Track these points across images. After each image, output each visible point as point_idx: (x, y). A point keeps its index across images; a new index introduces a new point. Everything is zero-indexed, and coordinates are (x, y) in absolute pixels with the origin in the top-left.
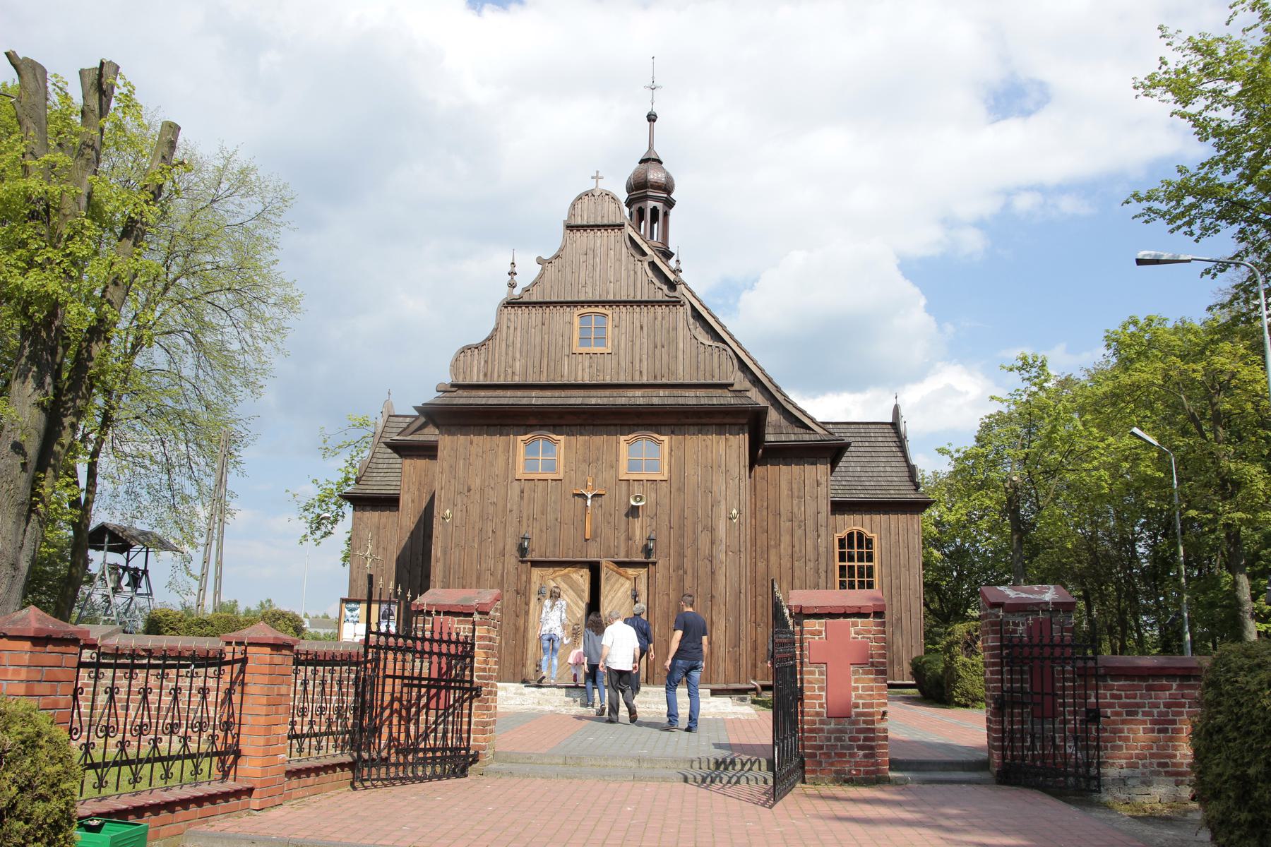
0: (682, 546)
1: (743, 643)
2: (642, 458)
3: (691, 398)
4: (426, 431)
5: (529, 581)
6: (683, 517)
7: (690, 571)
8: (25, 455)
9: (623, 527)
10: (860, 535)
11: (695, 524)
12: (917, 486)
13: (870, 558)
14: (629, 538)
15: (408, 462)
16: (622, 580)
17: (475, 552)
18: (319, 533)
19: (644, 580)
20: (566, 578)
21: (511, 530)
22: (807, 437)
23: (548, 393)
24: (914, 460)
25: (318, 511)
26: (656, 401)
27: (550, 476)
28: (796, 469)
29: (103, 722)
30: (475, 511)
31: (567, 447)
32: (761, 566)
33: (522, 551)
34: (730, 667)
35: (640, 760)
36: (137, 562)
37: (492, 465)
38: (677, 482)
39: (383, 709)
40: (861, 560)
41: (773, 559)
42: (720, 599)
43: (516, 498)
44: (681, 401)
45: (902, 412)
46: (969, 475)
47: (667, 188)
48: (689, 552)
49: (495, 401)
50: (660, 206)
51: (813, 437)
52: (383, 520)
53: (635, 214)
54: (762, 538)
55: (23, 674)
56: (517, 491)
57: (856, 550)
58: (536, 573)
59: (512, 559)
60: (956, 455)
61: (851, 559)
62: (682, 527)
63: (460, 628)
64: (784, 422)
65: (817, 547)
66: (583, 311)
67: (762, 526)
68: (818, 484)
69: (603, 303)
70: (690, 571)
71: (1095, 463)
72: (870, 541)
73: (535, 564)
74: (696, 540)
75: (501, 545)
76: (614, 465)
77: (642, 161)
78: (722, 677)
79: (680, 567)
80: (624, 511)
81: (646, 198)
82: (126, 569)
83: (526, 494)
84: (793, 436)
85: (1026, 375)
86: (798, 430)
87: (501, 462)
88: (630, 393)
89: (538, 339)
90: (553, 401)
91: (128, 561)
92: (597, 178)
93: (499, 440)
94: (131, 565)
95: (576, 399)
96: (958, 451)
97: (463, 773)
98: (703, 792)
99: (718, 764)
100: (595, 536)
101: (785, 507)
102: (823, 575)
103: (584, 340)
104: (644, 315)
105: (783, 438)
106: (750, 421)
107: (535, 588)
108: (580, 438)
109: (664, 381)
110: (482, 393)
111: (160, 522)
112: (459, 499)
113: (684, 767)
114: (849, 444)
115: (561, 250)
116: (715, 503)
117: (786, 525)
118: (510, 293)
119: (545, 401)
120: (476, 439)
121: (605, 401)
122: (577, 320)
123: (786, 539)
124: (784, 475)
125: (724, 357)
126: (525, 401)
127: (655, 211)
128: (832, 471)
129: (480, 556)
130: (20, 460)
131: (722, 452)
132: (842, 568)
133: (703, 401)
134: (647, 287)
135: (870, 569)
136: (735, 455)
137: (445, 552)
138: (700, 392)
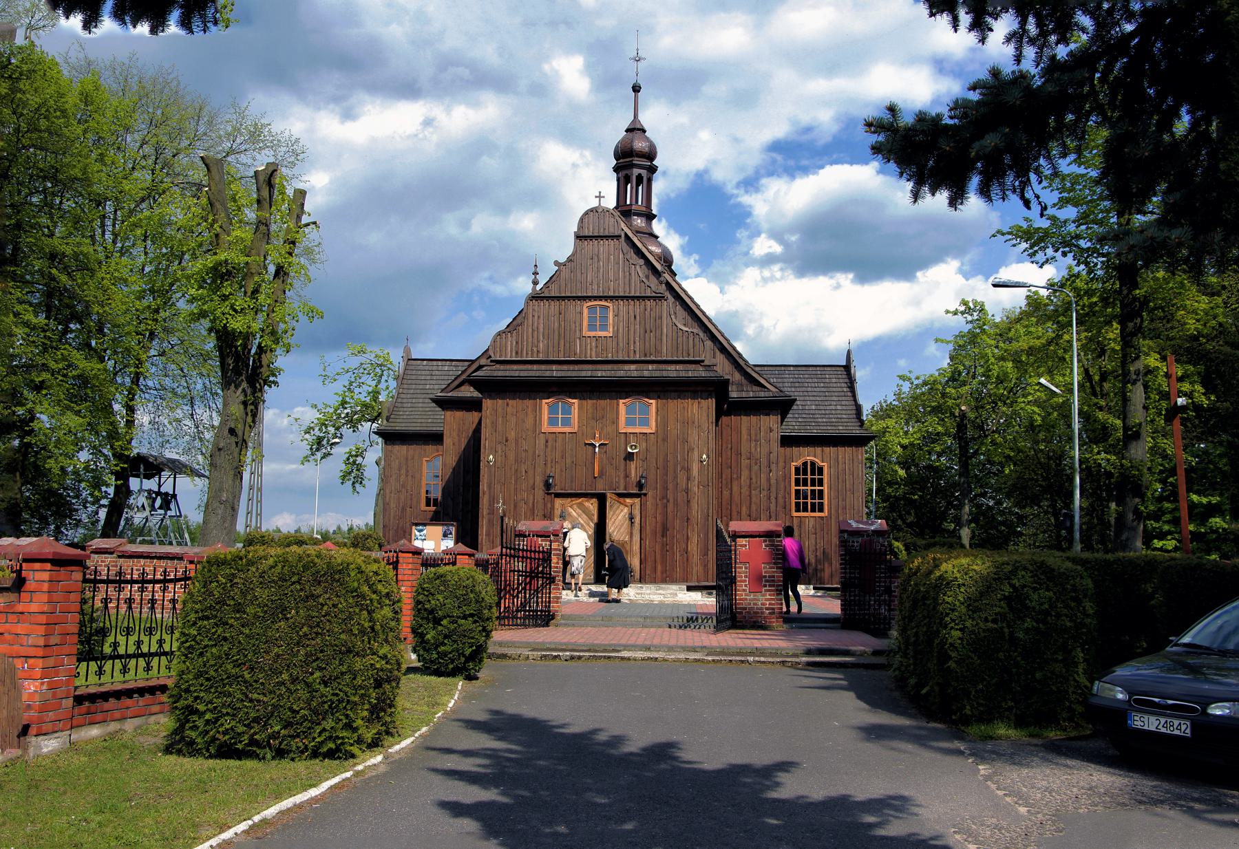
1: (710, 553)
2: (637, 419)
3: (672, 372)
5: (553, 508)
6: (666, 461)
9: (622, 468)
10: (813, 464)
11: (675, 466)
12: (862, 423)
13: (821, 483)
14: (627, 476)
15: (449, 413)
16: (622, 507)
17: (512, 487)
18: (319, 455)
19: (638, 507)
20: (580, 505)
21: (539, 470)
22: (762, 394)
23: (565, 367)
24: (861, 401)
26: (646, 374)
27: (567, 430)
28: (754, 419)
29: (126, 624)
30: (512, 456)
32: (726, 493)
33: (548, 486)
34: (701, 569)
36: (167, 488)
38: (663, 434)
40: (813, 484)
41: (735, 488)
42: (694, 521)
43: (543, 447)
45: (853, 357)
46: (929, 400)
47: (651, 155)
48: (670, 486)
49: (525, 374)
50: (644, 173)
51: (767, 394)
52: (411, 452)
53: (622, 179)
54: (727, 472)
57: (809, 477)
59: (540, 492)
61: (805, 484)
62: (666, 467)
63: (543, 544)
64: (744, 381)
65: (769, 480)
66: (590, 304)
67: (726, 465)
69: (606, 298)
72: (821, 470)
73: (558, 495)
74: (676, 477)
75: (531, 482)
76: (615, 421)
79: (664, 497)
80: (623, 456)
82: (158, 493)
83: (550, 444)
84: (751, 393)
85: (969, 318)
86: (756, 388)
87: (530, 420)
88: (627, 367)
91: (160, 486)
92: (600, 197)
94: (163, 490)
95: (586, 372)
96: (917, 378)
97: (547, 625)
98: (680, 631)
99: (688, 620)
100: (601, 474)
102: (773, 500)
103: (592, 327)
104: (637, 307)
105: (744, 394)
106: (715, 389)
107: (557, 512)
110: (515, 367)
112: (499, 448)
113: (669, 621)
114: (793, 401)
115: (573, 255)
116: (691, 450)
117: (745, 462)
118: (534, 289)
120: (511, 402)
122: (586, 311)
123: (745, 473)
124: (745, 422)
125: (697, 340)
128: (782, 421)
129: (516, 489)
132: (797, 492)
133: (683, 374)
134: (638, 279)
135: (821, 492)
136: (705, 414)
137: (489, 487)
138: (678, 367)
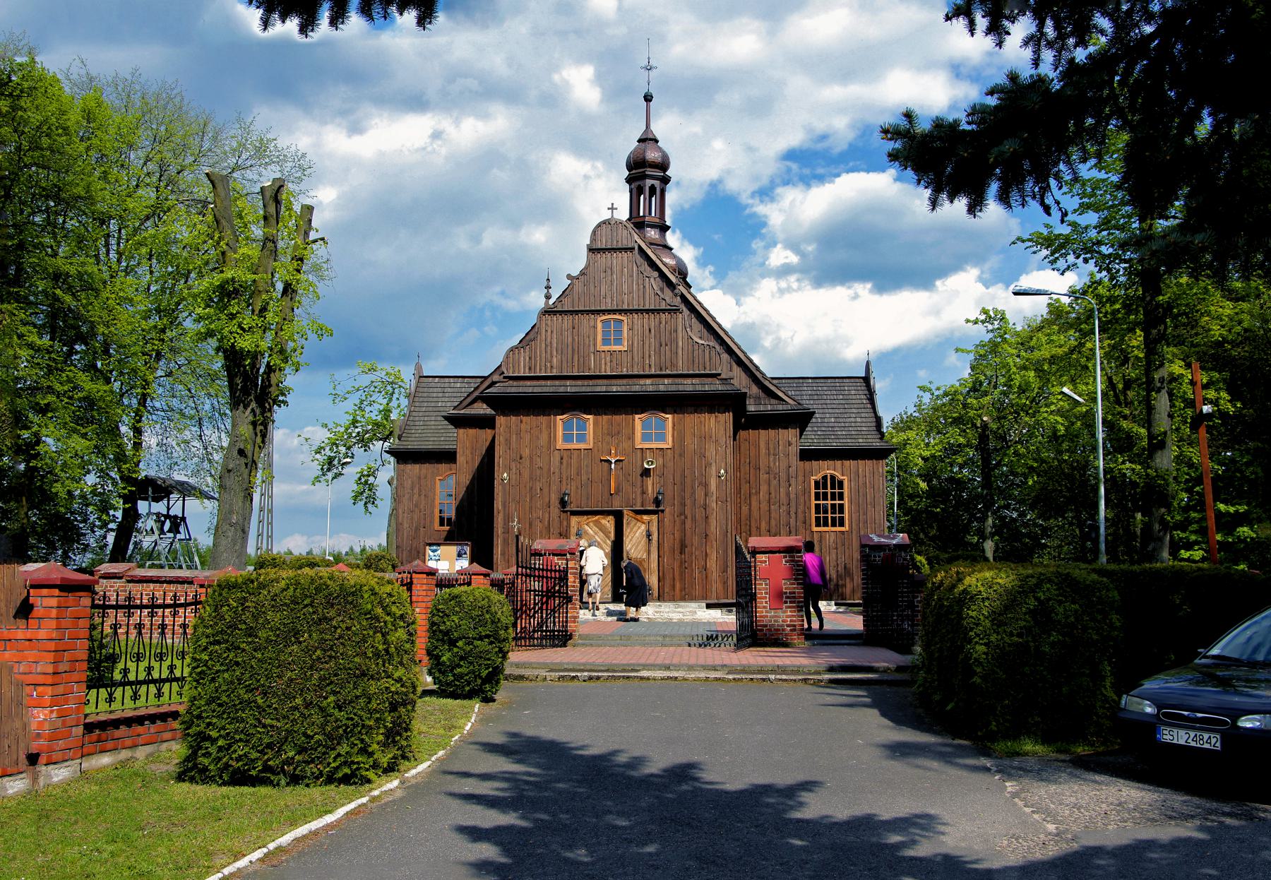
0: (683, 498)
2: (653, 434)
4: (475, 405)
5: (569, 526)
7: (689, 517)
8: (246, 456)
9: (639, 484)
10: (833, 477)
11: (693, 481)
14: (643, 493)
15: (461, 431)
18: (330, 475)
19: (655, 524)
20: (597, 523)
22: (780, 407)
23: (579, 383)
24: (881, 413)
25: (329, 453)
26: (662, 388)
27: (582, 446)
28: (772, 432)
30: (526, 474)
31: (595, 424)
32: (745, 509)
33: (563, 503)
34: (720, 586)
35: (664, 636)
36: (176, 511)
37: (538, 438)
38: (680, 448)
39: (541, 608)
40: (833, 498)
41: (754, 503)
42: (712, 537)
43: (557, 464)
44: (681, 388)
46: (950, 412)
47: (663, 166)
48: (688, 502)
50: (657, 183)
51: (785, 407)
52: (424, 471)
53: (635, 191)
54: (745, 487)
55: (425, 587)
56: (558, 458)
57: (829, 491)
58: (574, 520)
59: (555, 510)
60: (936, 393)
61: (825, 498)
62: (683, 484)
63: (560, 562)
64: (762, 395)
65: (788, 494)
67: (744, 482)
68: (790, 444)
69: (620, 311)
70: (689, 517)
71: (1053, 408)
72: (841, 484)
73: (574, 513)
74: (693, 493)
76: (631, 437)
77: (639, 141)
78: (714, 595)
79: (682, 513)
80: (639, 472)
81: (644, 177)
83: (564, 461)
84: (769, 406)
85: (990, 327)
86: (773, 401)
87: (545, 436)
88: (642, 382)
89: (570, 339)
90: (583, 389)
91: (169, 509)
92: (612, 208)
93: (543, 419)
94: (172, 513)
95: (601, 388)
96: (938, 389)
97: (564, 645)
98: (701, 650)
99: (708, 638)
100: (618, 491)
101: (763, 463)
103: (606, 341)
104: (652, 320)
105: (762, 408)
107: (573, 530)
108: (605, 417)
109: (668, 372)
110: (528, 383)
111: (196, 473)
113: (689, 640)
115: (586, 268)
117: (764, 477)
118: (547, 303)
119: (577, 389)
120: (524, 419)
121: (624, 388)
122: (599, 325)
123: (764, 488)
125: (713, 353)
126: (562, 389)
127: (652, 189)
128: (801, 435)
130: (243, 460)
131: (712, 425)
132: (817, 506)
135: (841, 506)
138: (695, 381)
